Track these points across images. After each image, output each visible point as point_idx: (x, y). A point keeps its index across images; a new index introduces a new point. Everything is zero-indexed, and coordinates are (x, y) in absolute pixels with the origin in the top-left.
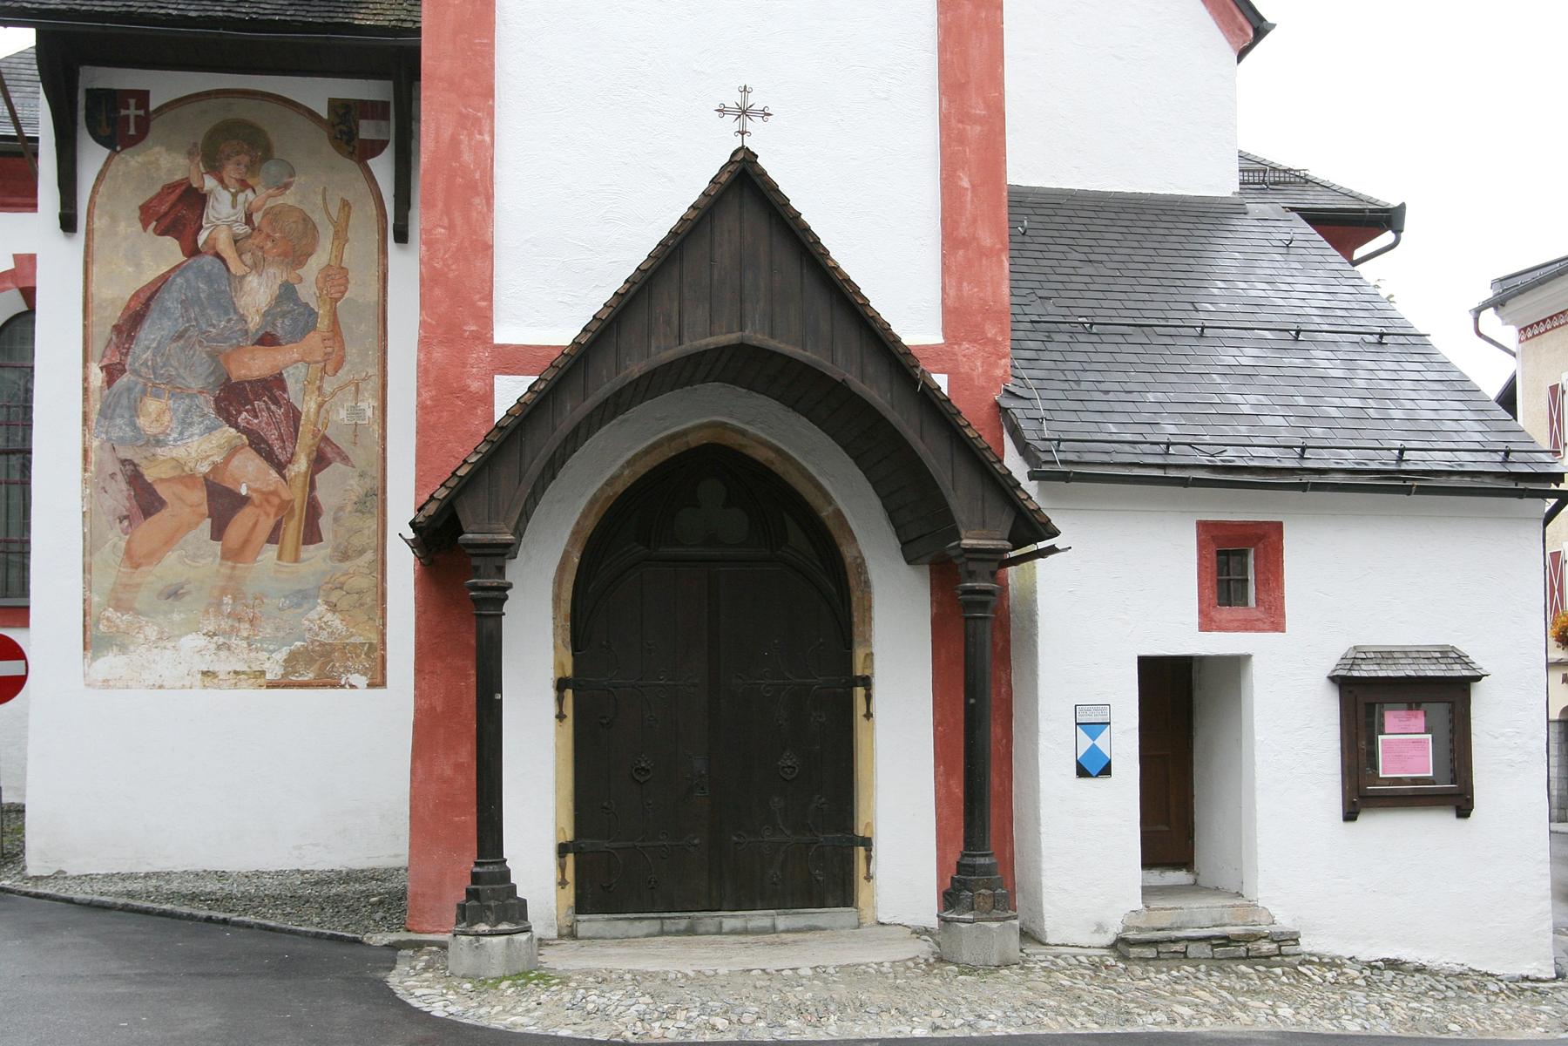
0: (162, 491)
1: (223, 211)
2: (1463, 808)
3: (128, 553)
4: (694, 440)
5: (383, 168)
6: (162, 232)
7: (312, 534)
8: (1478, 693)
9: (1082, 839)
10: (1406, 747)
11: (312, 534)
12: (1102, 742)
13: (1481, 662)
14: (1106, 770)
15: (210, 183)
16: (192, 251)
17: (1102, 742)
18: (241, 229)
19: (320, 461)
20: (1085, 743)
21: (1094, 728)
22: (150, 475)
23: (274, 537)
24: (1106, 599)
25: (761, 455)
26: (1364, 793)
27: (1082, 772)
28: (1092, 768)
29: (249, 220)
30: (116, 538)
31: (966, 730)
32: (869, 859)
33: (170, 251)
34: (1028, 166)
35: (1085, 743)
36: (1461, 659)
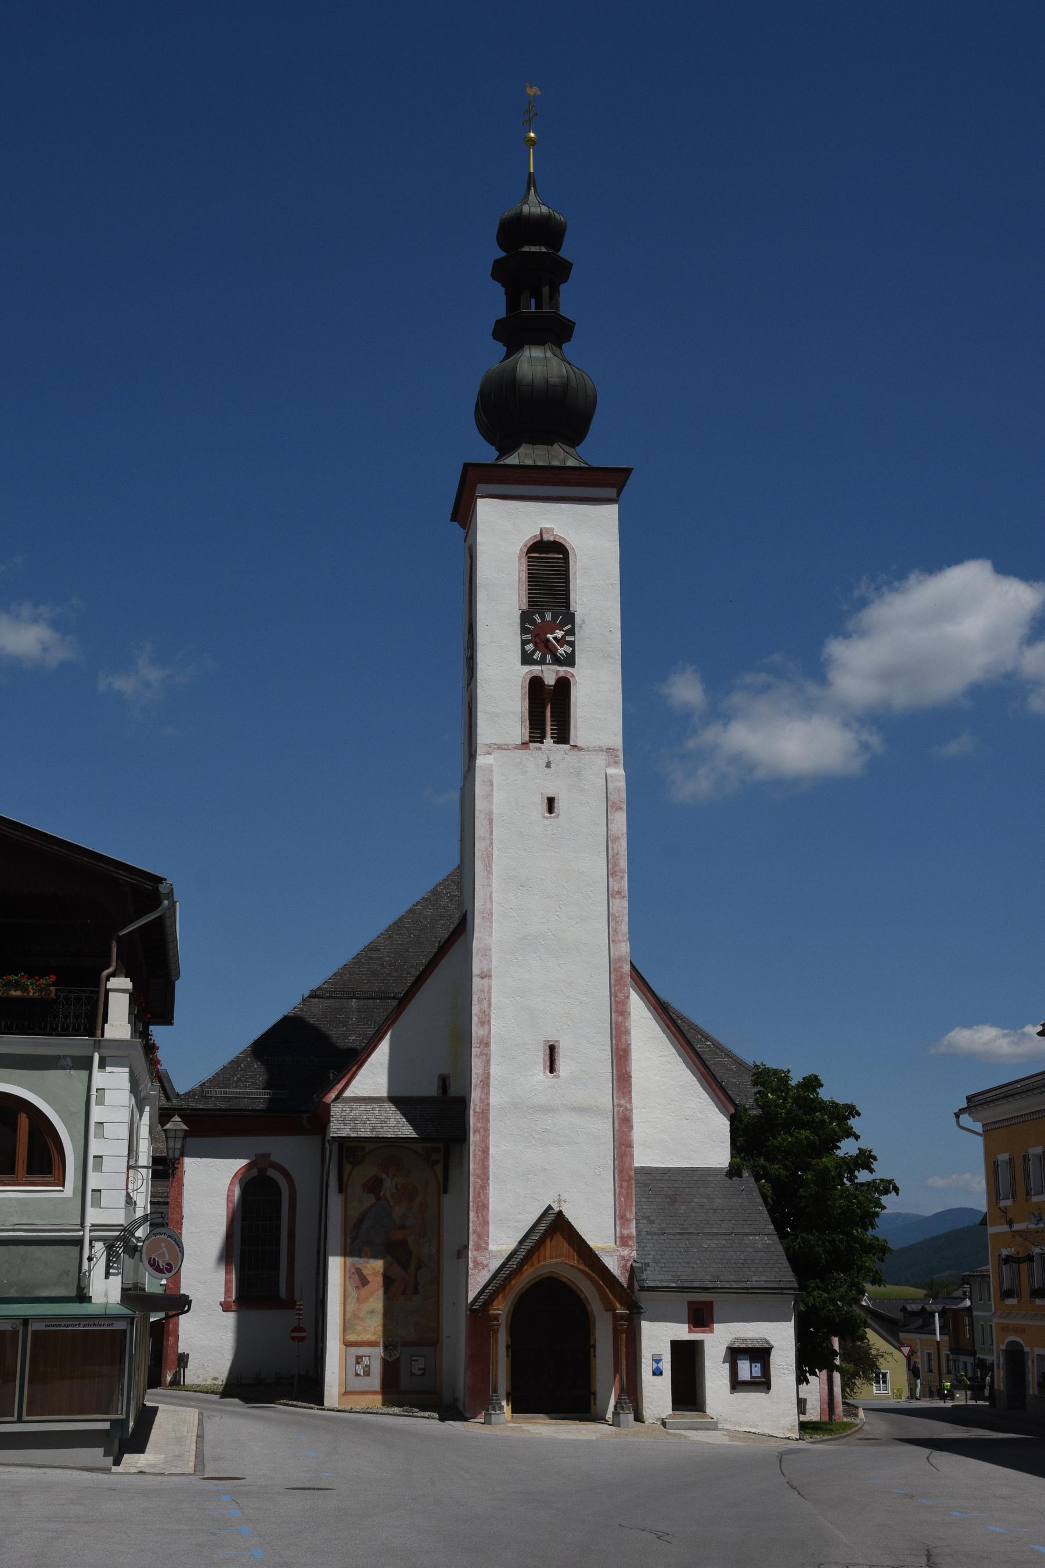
0: (369, 1278)
1: (388, 1184)
2: (769, 1387)
3: (358, 1299)
4: (544, 1276)
5: (439, 1169)
6: (369, 1192)
7: (416, 1292)
8: (773, 1352)
9: (657, 1392)
10: (746, 1369)
11: (416, 1292)
12: (660, 1365)
13: (773, 1343)
14: (661, 1374)
15: (384, 1176)
16: (378, 1198)
17: (660, 1365)
18: (394, 1191)
19: (419, 1267)
20: (655, 1365)
21: (658, 1361)
22: (365, 1272)
23: (404, 1293)
24: (657, 1338)
25: (563, 1279)
26: (736, 1385)
27: (654, 1374)
28: (657, 1373)
29: (396, 1187)
30: (353, 1293)
31: (583, 1242)
32: (595, 1399)
33: (370, 1200)
34: (642, 1158)
35: (655, 1365)
36: (767, 1342)
